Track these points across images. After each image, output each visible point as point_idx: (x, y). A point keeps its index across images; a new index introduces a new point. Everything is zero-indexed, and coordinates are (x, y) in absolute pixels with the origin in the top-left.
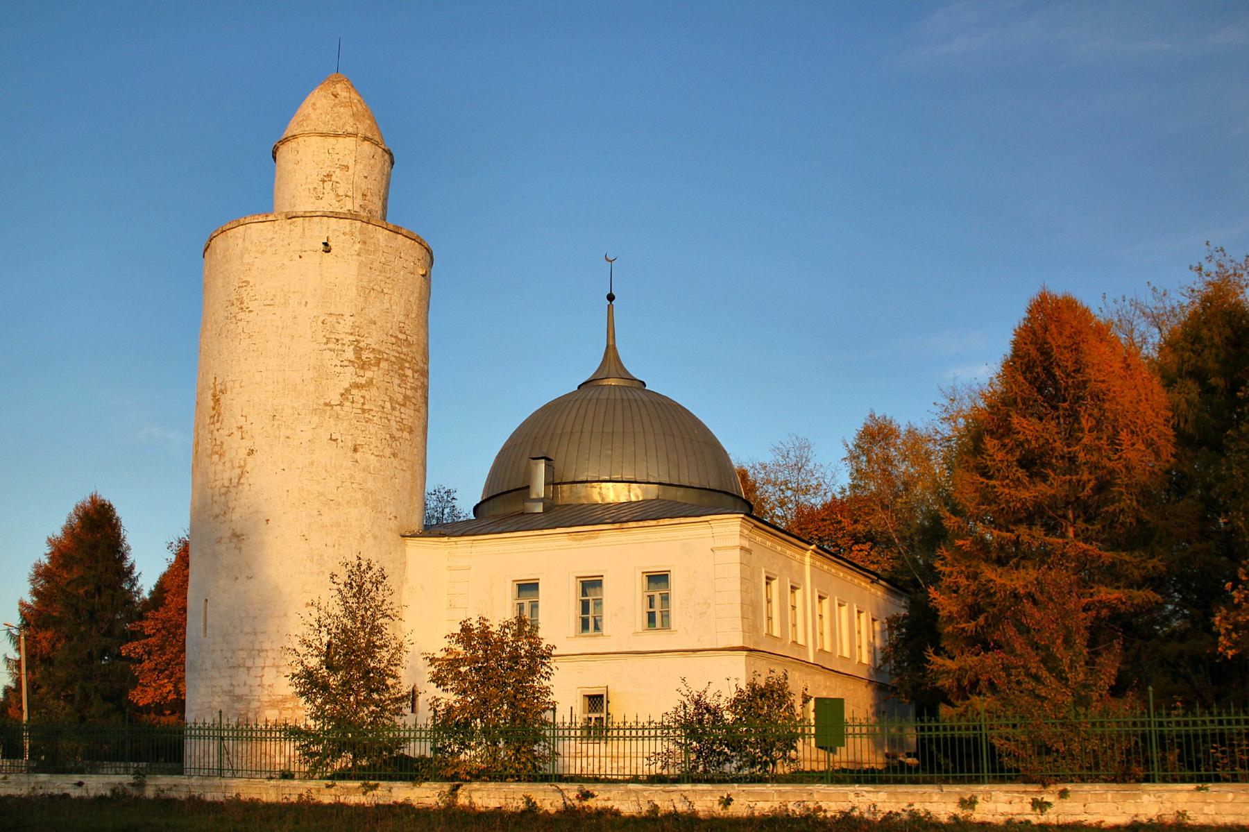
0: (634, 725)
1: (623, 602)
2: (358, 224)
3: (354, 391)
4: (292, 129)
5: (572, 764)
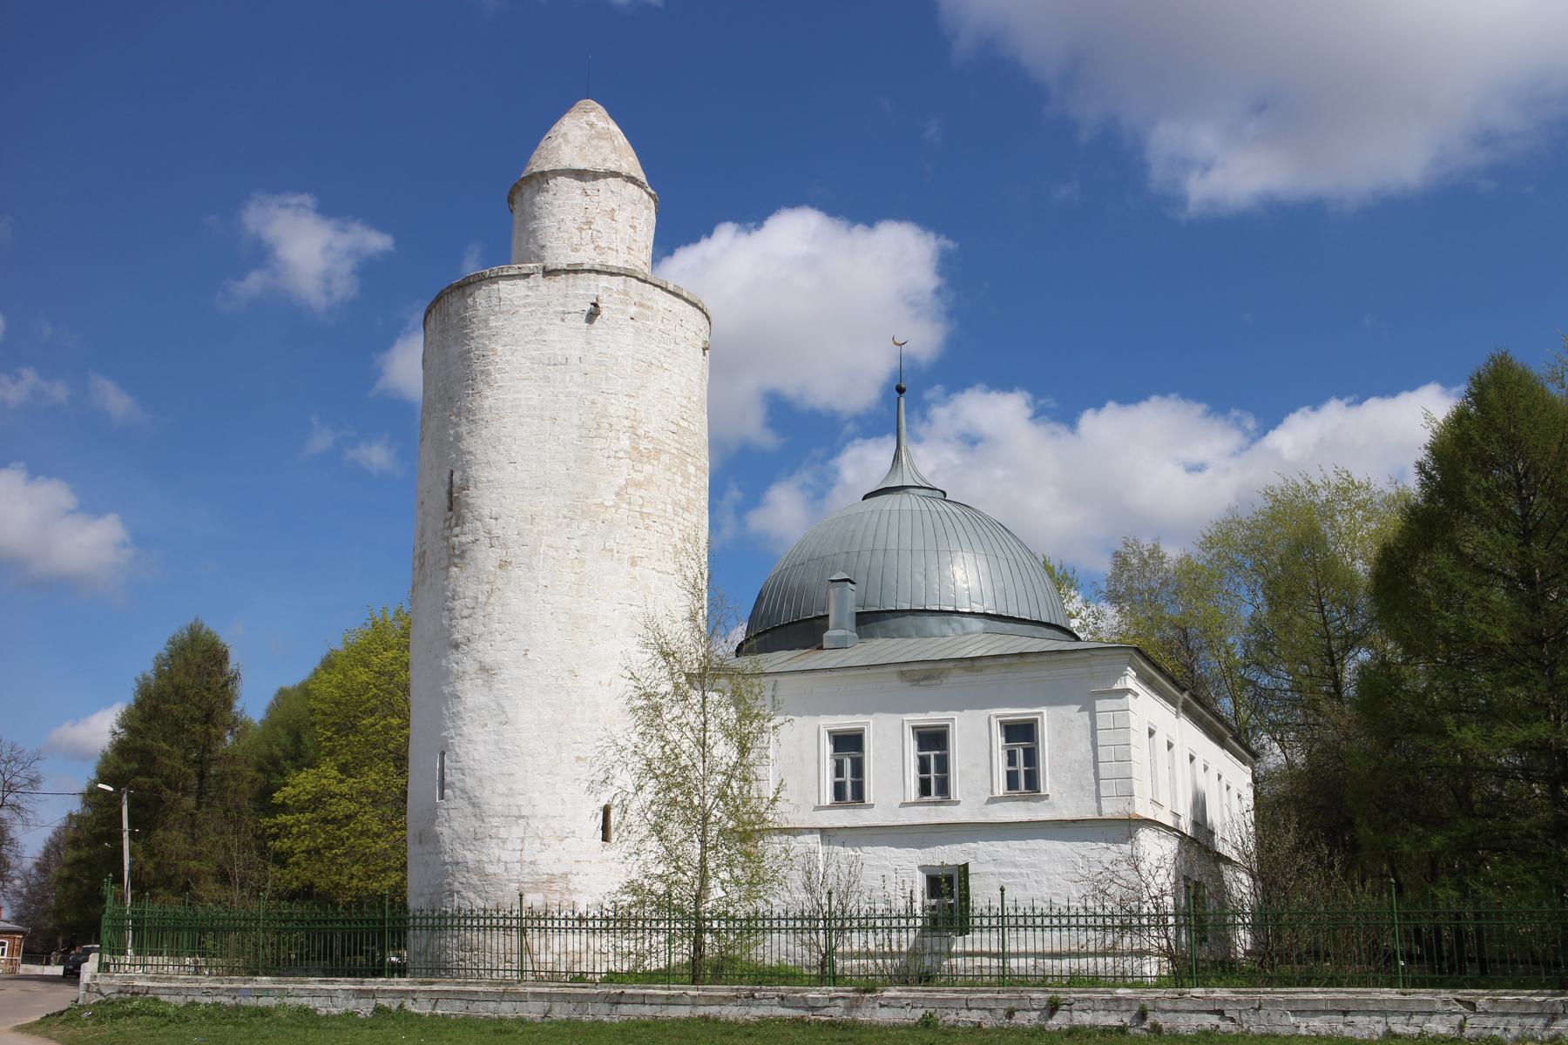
0: (985, 912)
4: (538, 163)
5: (791, 947)
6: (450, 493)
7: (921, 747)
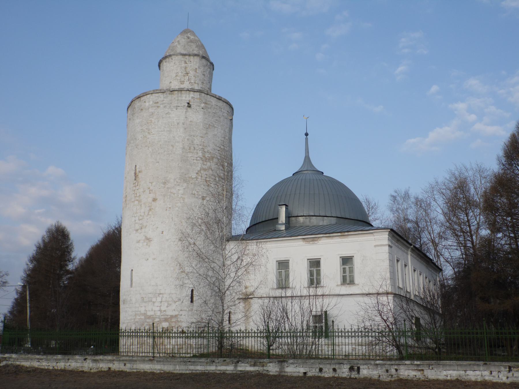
1: (331, 271)
2: (203, 95)
3: (202, 172)
6: (135, 174)
7: (311, 267)
